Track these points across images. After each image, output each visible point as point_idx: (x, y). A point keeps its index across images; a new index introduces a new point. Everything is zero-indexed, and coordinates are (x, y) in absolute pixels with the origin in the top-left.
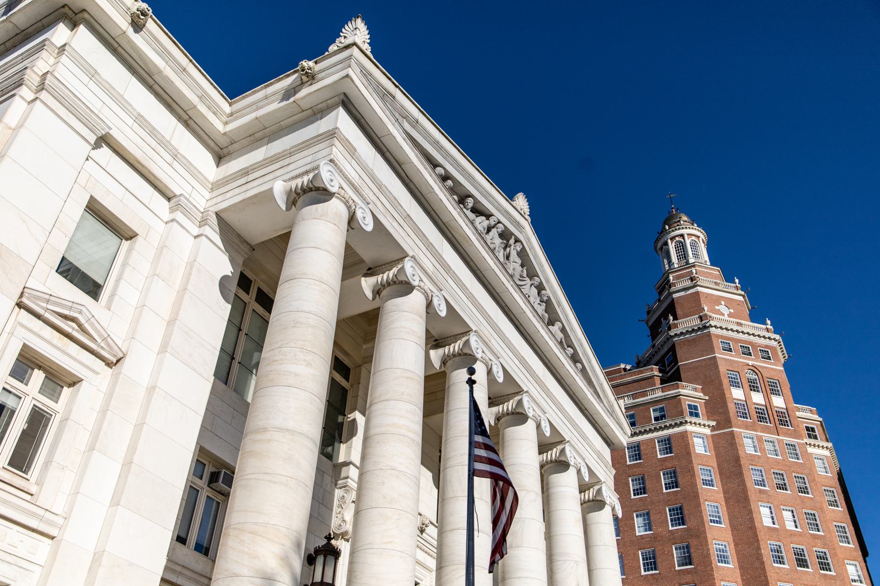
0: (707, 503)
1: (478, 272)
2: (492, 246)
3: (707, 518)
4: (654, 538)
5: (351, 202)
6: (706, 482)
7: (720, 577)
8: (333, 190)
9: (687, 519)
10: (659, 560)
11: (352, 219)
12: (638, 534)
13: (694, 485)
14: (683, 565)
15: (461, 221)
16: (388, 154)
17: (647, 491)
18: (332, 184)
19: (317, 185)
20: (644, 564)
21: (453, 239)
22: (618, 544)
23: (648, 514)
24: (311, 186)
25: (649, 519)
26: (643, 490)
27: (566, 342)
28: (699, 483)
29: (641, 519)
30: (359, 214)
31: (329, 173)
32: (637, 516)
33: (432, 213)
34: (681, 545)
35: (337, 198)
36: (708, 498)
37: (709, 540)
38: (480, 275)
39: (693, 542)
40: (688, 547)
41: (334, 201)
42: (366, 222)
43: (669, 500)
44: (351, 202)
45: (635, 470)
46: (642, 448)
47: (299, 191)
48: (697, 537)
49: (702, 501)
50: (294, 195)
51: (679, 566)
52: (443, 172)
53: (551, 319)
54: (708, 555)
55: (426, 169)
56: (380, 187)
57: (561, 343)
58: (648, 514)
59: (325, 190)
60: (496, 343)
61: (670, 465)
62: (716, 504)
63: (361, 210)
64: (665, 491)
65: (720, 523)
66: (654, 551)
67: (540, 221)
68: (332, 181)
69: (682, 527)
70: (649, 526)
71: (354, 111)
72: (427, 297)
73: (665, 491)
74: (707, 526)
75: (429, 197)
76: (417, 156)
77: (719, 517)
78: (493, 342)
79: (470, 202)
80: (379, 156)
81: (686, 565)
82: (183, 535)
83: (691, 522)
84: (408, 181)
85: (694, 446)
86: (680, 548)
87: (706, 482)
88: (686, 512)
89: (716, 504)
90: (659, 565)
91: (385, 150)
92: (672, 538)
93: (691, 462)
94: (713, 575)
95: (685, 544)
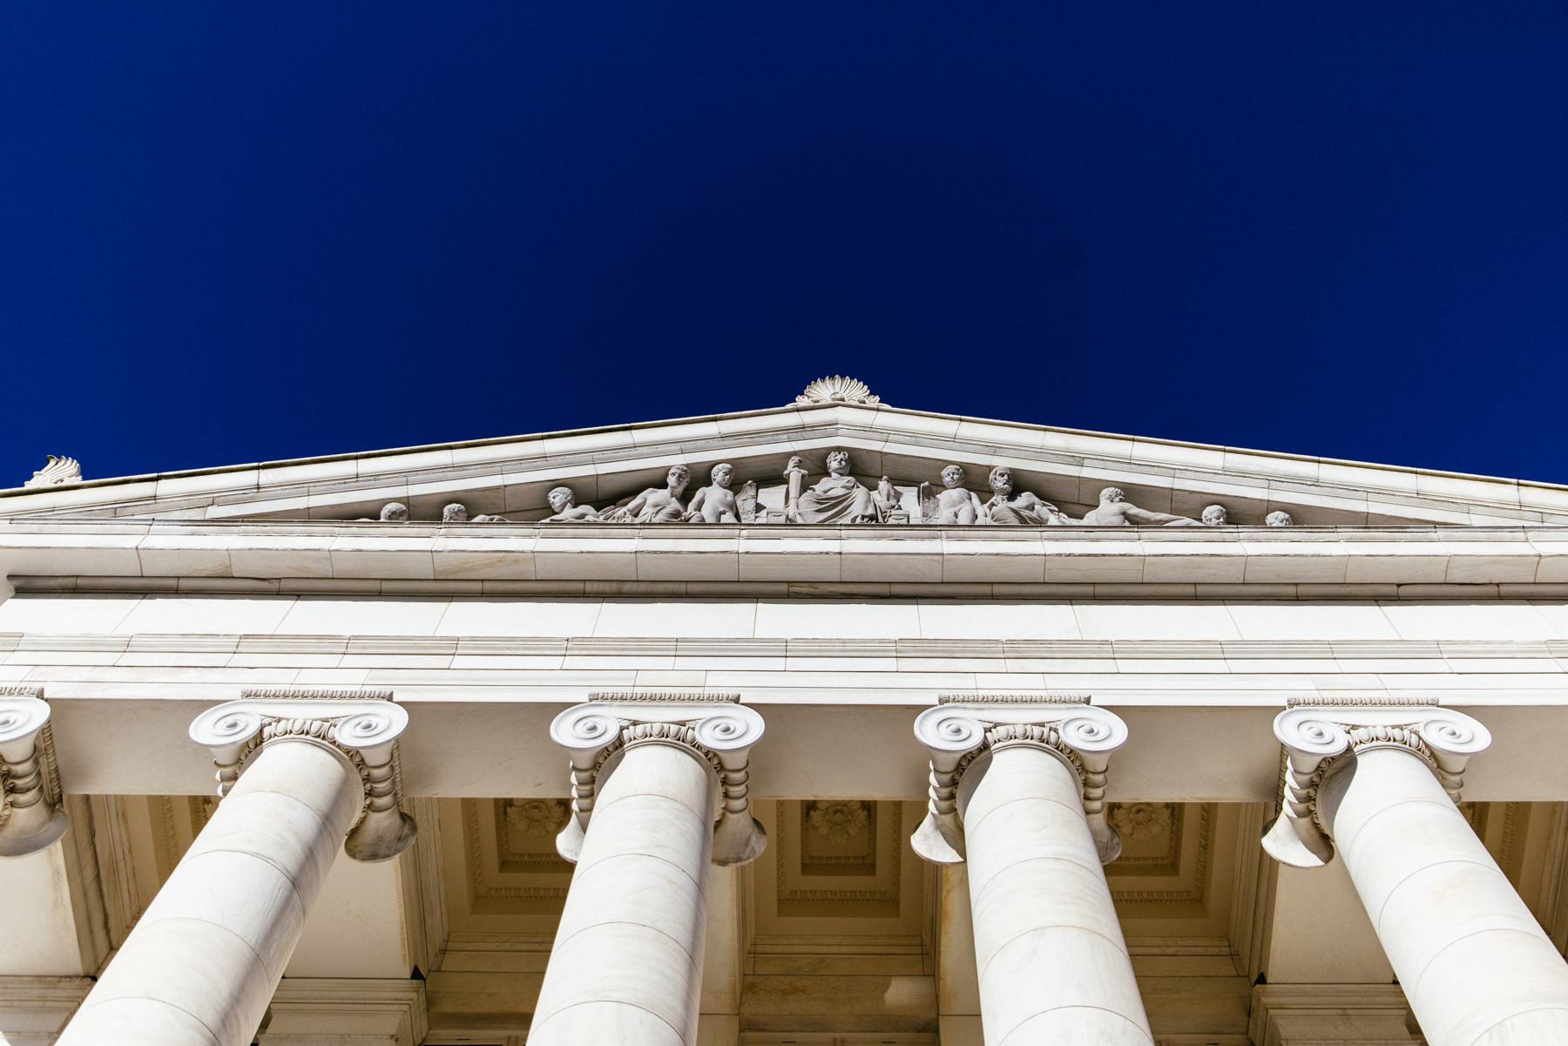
1: (627, 588)
2: (782, 520)
5: (1037, 731)
8: (1337, 748)
11: (1435, 761)
15: (743, 545)
16: (184, 584)
18: (1327, 738)
19: (951, 767)
21: (488, 586)
24: (1305, 778)
27: (1146, 505)
30: (1438, 739)
31: (1304, 727)
33: (386, 586)
35: (1364, 752)
38: (642, 588)
41: (1367, 765)
42: (1465, 737)
44: (1397, 733)
47: (1302, 807)
50: (1305, 822)
52: (1281, 515)
53: (1071, 500)
55: (290, 534)
56: (94, 645)
57: (1134, 522)
59: (1330, 760)
60: (1355, 680)
63: (1433, 728)
67: (898, 390)
68: (1321, 734)
71: (52, 583)
72: (1403, 746)
75: (528, 571)
76: (246, 534)
78: (713, 679)
79: (558, 497)
80: (763, 607)
84: (275, 585)
91: (172, 583)
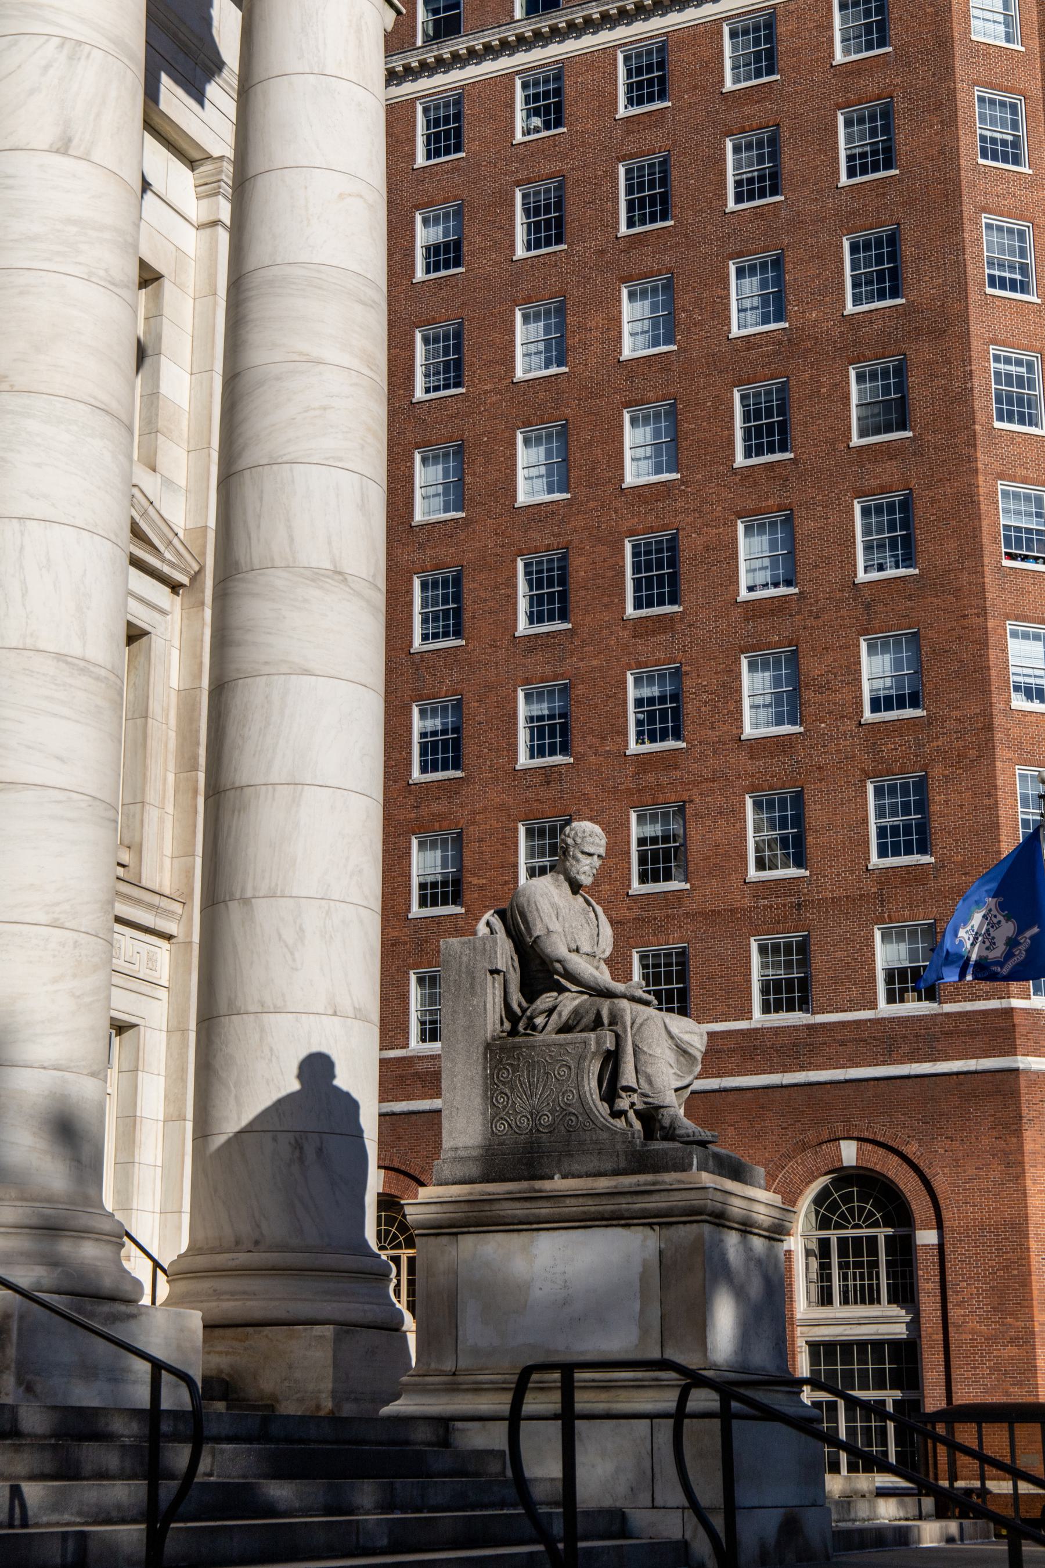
0: (985, 219)
3: (979, 271)
4: (787, 345)
6: (991, 149)
7: (997, 467)
9: (908, 272)
10: (796, 416)
12: (735, 332)
13: (948, 156)
14: (877, 431)
17: (784, 183)
20: (747, 432)
22: (386, 41)
23: (778, 263)
25: (779, 281)
26: (919, 839)
28: (968, 147)
29: (752, 285)
32: (740, 273)
34: (878, 364)
36: (992, 202)
37: (975, 344)
39: (921, 353)
40: (900, 371)
43: (854, 213)
45: (748, 110)
46: (782, 29)
48: (938, 334)
49: (968, 209)
51: (862, 434)
54: (966, 394)
58: (778, 263)
61: (873, 89)
62: (1016, 224)
64: (875, 861)
65: (1024, 288)
66: (783, 389)
69: (888, 303)
70: (775, 305)
73: (875, 861)
74: (973, 296)
77: (1024, 269)
81: (888, 430)
82: (789, 578)
83: (921, 286)
85: (966, 16)
86: (873, 376)
87: (991, 149)
88: (907, 250)
89: (1016, 224)
90: (796, 434)
92: (852, 342)
93: (950, 71)
94: (972, 459)
95: (891, 362)
